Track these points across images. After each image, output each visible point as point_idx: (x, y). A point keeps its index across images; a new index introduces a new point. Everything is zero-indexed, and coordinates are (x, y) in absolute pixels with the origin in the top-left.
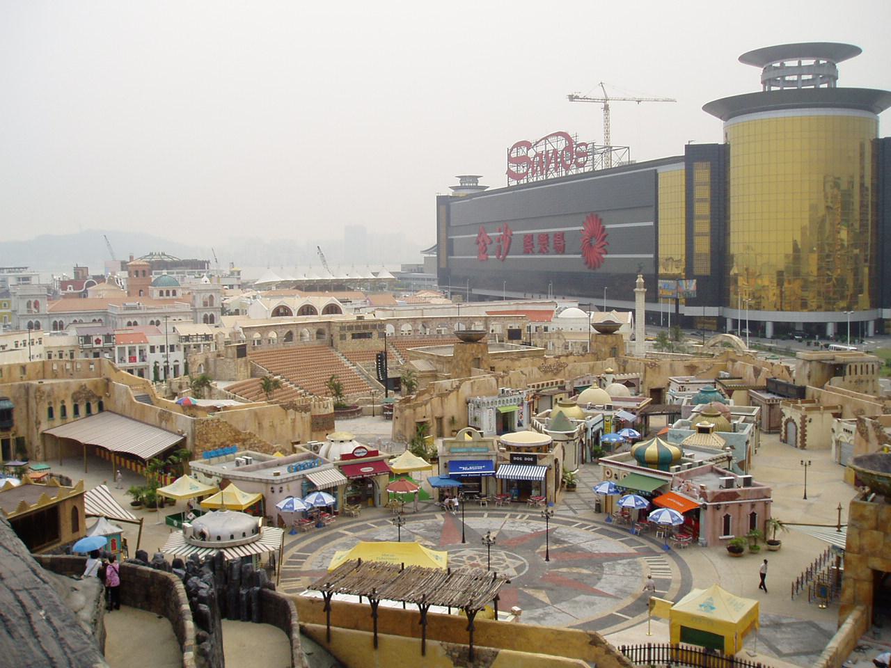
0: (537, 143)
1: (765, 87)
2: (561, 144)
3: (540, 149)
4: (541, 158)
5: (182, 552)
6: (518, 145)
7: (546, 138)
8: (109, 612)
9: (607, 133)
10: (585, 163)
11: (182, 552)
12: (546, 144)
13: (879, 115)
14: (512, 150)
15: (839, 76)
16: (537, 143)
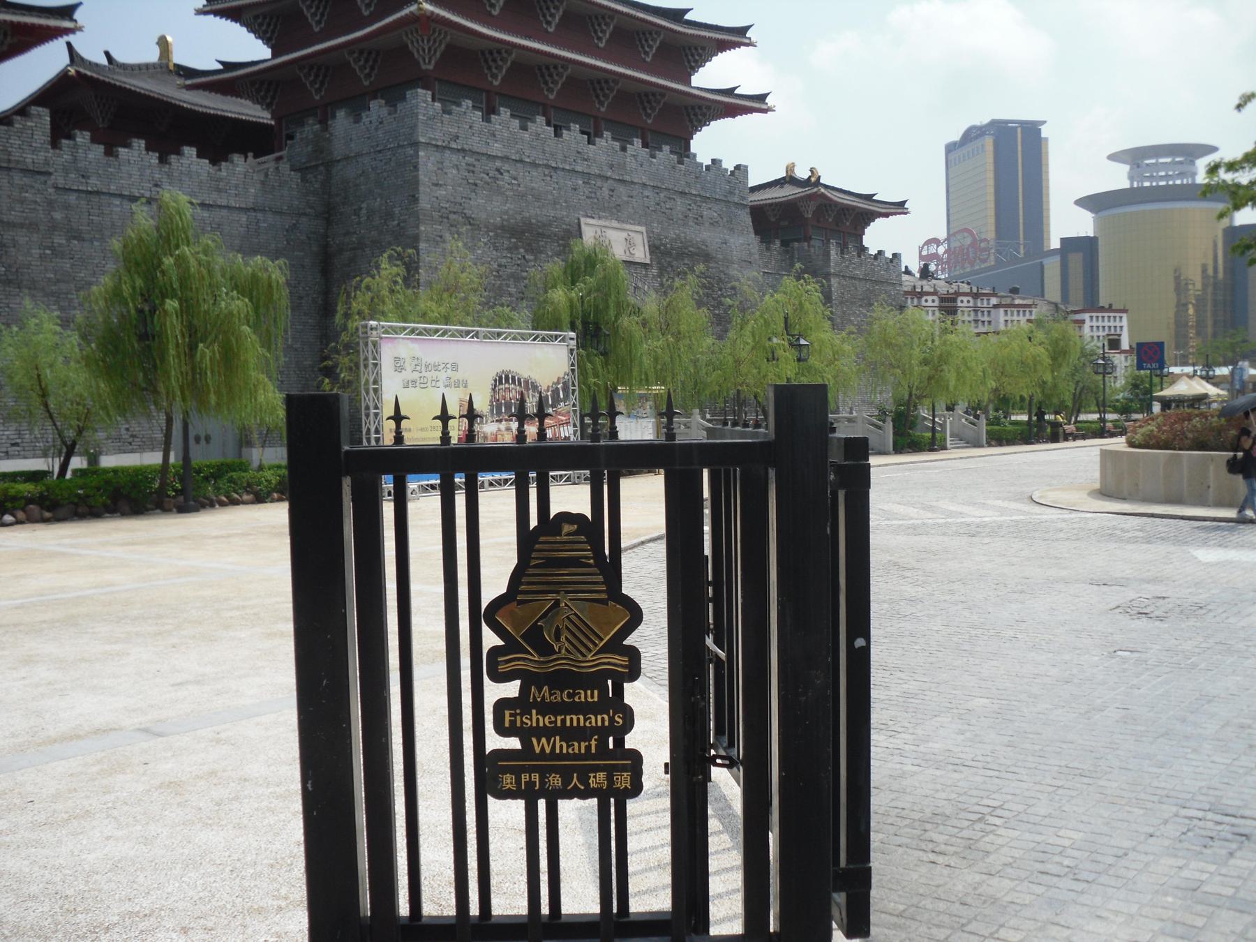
1: (1132, 184)
5: (589, 578)
11: (589, 578)
14: (923, 248)
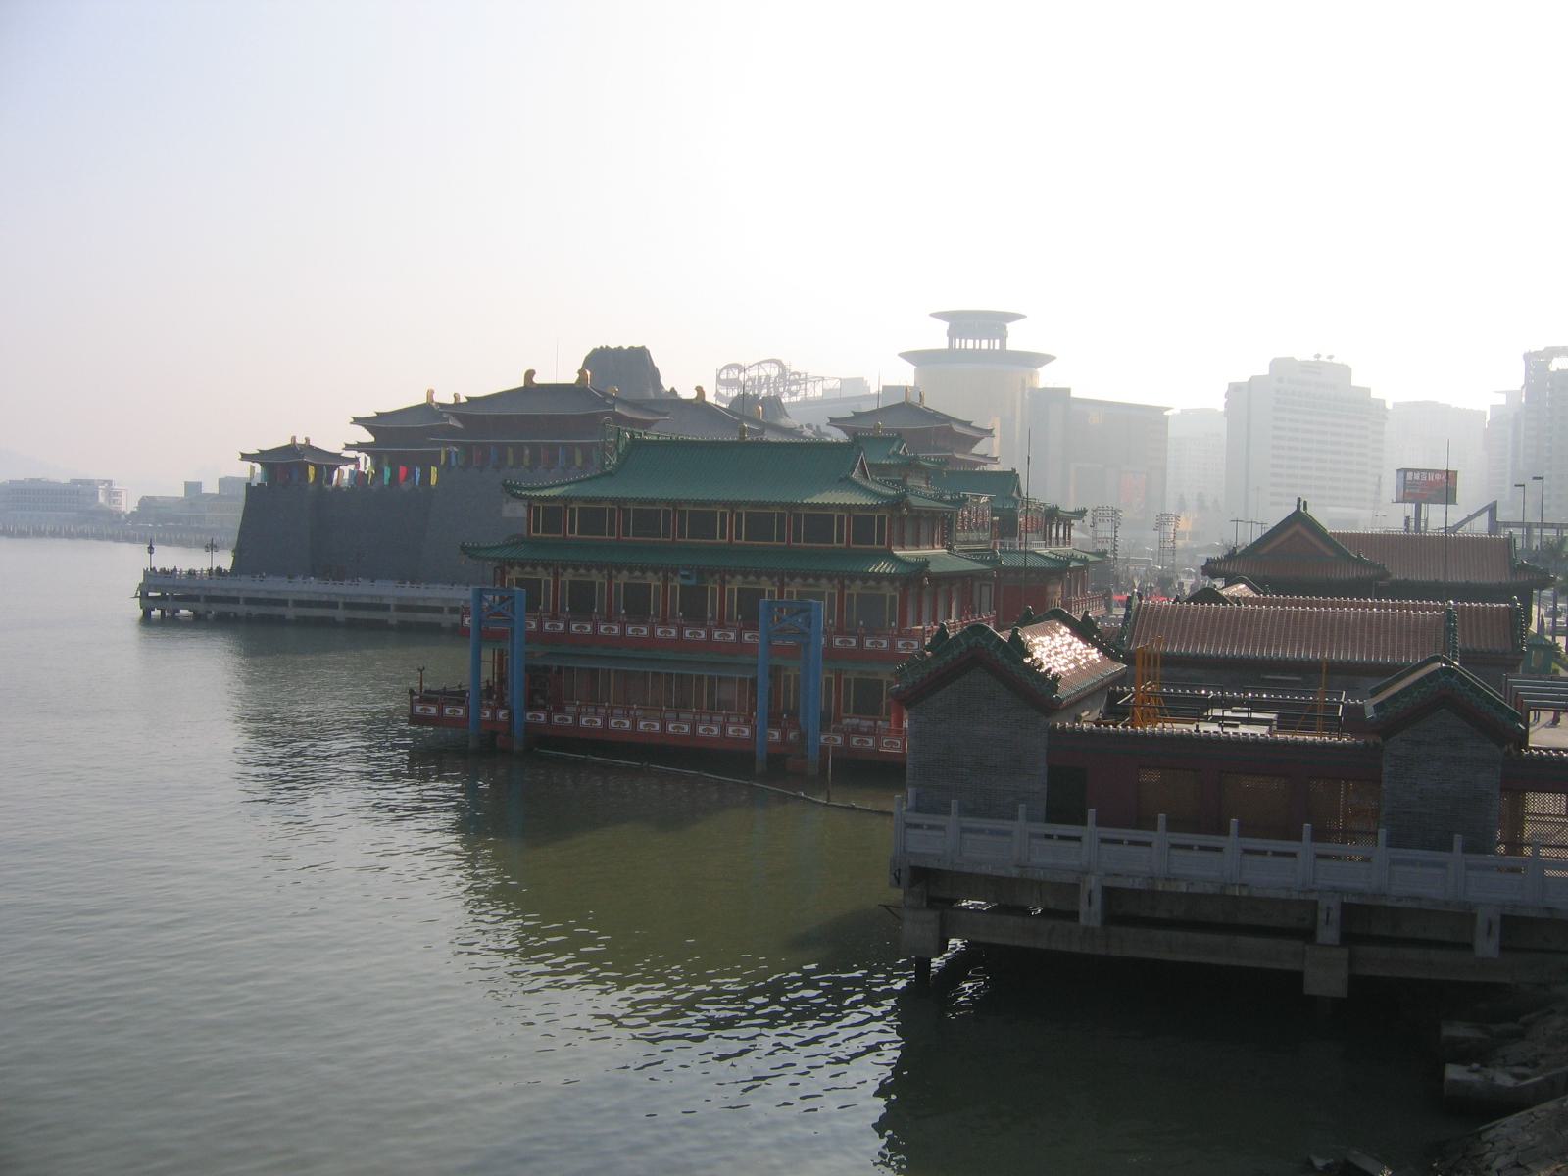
0: (750, 367)
2: (774, 372)
3: (753, 373)
4: (753, 382)
6: (729, 367)
7: (759, 364)
10: (798, 391)
13: (1039, 370)
14: (722, 371)
16: (750, 367)
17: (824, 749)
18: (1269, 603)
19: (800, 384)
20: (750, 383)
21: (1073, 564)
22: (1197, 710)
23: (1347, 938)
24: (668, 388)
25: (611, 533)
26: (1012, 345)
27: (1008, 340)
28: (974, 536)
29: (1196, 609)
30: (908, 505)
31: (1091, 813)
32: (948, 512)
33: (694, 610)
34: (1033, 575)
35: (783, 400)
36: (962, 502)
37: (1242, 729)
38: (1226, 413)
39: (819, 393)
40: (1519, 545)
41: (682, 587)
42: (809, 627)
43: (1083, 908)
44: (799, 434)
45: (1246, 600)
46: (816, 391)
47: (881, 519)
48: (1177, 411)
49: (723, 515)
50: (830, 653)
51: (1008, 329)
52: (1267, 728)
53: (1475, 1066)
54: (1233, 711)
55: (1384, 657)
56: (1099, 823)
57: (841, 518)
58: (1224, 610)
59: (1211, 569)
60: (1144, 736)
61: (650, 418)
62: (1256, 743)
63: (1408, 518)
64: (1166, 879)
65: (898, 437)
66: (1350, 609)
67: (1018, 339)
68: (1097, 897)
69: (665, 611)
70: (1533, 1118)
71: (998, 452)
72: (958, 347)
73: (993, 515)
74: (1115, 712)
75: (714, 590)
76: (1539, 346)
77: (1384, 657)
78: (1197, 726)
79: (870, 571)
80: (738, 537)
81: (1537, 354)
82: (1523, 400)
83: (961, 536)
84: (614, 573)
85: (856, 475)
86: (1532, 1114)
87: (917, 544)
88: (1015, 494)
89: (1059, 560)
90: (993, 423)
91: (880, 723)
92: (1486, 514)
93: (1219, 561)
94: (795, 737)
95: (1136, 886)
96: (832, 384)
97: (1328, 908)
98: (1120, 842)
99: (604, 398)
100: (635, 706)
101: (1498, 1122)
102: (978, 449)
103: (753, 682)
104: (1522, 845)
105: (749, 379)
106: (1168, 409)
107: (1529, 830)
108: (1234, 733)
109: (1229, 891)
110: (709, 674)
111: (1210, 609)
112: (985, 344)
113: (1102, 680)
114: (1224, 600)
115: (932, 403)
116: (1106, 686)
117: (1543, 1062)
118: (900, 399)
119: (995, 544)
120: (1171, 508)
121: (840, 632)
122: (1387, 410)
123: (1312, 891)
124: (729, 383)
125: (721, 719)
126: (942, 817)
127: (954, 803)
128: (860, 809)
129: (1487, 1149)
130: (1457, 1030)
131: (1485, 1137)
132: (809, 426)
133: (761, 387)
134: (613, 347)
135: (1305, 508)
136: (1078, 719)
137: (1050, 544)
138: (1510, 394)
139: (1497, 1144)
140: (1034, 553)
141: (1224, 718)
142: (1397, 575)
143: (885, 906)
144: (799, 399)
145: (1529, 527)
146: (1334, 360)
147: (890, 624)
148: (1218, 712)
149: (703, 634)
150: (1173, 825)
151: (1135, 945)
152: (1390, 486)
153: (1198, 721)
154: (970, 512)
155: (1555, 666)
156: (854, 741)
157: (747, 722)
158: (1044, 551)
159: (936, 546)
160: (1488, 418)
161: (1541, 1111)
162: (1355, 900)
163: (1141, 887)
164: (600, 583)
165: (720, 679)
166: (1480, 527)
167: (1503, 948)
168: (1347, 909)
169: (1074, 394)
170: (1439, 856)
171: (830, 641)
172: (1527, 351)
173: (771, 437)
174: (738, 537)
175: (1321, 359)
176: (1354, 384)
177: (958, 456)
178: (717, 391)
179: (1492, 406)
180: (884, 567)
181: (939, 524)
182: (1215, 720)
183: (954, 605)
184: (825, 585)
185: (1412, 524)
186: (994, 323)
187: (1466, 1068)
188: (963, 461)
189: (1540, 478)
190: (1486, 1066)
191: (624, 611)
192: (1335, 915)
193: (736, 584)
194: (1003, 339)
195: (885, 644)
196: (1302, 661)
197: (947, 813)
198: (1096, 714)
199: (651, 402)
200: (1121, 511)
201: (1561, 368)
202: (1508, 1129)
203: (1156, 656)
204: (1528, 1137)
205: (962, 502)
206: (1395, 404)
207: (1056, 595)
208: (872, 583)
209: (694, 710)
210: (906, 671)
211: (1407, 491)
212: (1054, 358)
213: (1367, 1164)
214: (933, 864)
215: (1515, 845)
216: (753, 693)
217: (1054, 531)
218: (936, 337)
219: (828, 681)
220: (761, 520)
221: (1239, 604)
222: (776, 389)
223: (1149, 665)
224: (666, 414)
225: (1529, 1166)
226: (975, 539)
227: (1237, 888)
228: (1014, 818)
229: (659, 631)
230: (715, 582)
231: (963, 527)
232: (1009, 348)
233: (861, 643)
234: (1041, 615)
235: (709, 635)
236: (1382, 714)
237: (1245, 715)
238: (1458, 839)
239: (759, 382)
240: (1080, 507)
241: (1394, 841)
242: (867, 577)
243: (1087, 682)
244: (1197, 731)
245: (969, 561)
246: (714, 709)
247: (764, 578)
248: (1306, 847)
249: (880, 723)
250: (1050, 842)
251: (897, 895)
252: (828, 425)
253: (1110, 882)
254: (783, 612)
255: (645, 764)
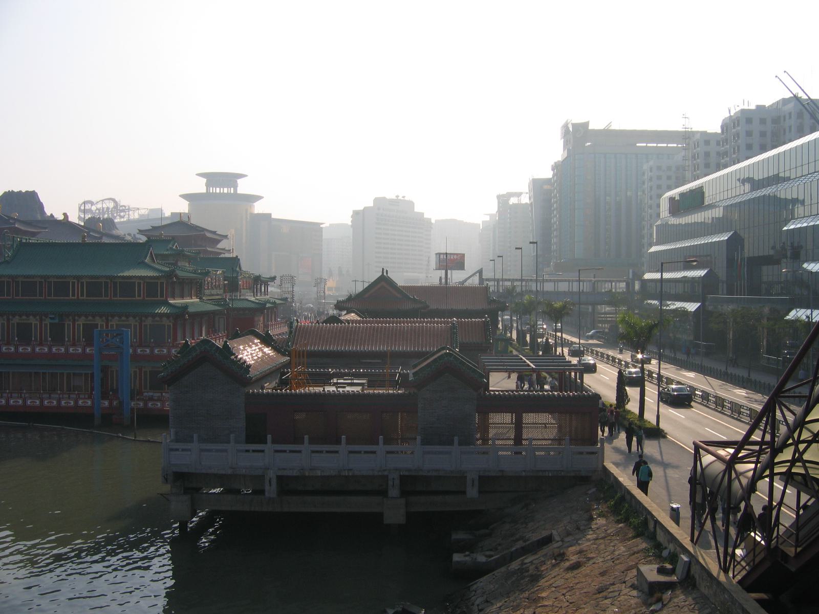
0: (97, 202)
2: (111, 205)
3: (99, 206)
7: (103, 201)
8: (260, 276)
9: (791, 92)
10: (124, 216)
12: (102, 204)
14: (81, 205)
15: (781, 98)
17: (132, 409)
18: (366, 322)
19: (126, 212)
20: (98, 211)
21: (268, 305)
22: (325, 379)
23: (404, 493)
24: (48, 214)
25: (106, 296)
26: (240, 191)
27: (238, 188)
28: (214, 292)
29: (326, 327)
30: (176, 276)
31: (269, 437)
32: (200, 279)
33: (58, 336)
34: (247, 312)
35: (116, 221)
36: (207, 274)
37: (348, 389)
38: (352, 226)
39: (136, 216)
40: (491, 290)
41: (50, 323)
42: (123, 344)
43: (267, 488)
44: (123, 239)
45: (356, 322)
46: (135, 216)
47: (162, 284)
48: (328, 225)
49: (73, 283)
50: (135, 357)
51: (238, 182)
52: (361, 387)
53: (467, 553)
54: (344, 380)
55: (422, 348)
56: (274, 442)
57: (139, 284)
58: (341, 327)
59: (339, 306)
60: (301, 394)
61: (36, 231)
62: (354, 396)
63: (441, 278)
64: (310, 469)
65: (173, 240)
66: (406, 324)
67: (243, 187)
68: (274, 481)
69: (74, 338)
70: (494, 577)
71: (230, 246)
72: (211, 191)
73: (225, 280)
74: (283, 383)
75: (69, 325)
76: (503, 192)
77: (422, 348)
78: (324, 389)
79: (156, 312)
80: (82, 295)
81: (503, 196)
82: (497, 218)
83: (207, 292)
84: (10, 317)
85: (147, 260)
86: (494, 575)
87: (182, 297)
88: (238, 269)
89: (261, 304)
90: (231, 233)
91: (164, 394)
92: (478, 274)
93: (343, 302)
94: (116, 404)
95: (295, 475)
96: (143, 212)
97: (393, 479)
98: (285, 451)
99: (9, 220)
100: (25, 391)
101: (477, 581)
102: (220, 246)
103: (92, 375)
104: (488, 440)
105: (97, 209)
106: (322, 224)
107: (492, 433)
108: (343, 391)
109: (343, 474)
110: (61, 371)
111: (334, 327)
112: (226, 190)
113: (276, 366)
114: (341, 322)
115: (194, 221)
116: (280, 368)
117: (499, 548)
118: (178, 219)
119: (226, 296)
120: (325, 276)
121: (140, 346)
122: (432, 224)
123: (384, 470)
124: (84, 211)
125: (75, 396)
126: (226, 445)
127: (195, 436)
128: (152, 442)
129: (472, 595)
130: (459, 535)
131: (471, 589)
132: (129, 234)
133: (104, 213)
134: (16, 191)
135: (387, 273)
136: (263, 388)
137: (257, 295)
138: (491, 215)
139: (478, 592)
140: (247, 300)
141: (337, 383)
142: (433, 306)
143: (161, 494)
144: (125, 219)
145: (498, 281)
146: (406, 199)
147: (168, 340)
148: (335, 380)
149: (63, 349)
150: (312, 441)
151: (295, 505)
152: (433, 264)
153: (324, 386)
154: (212, 279)
155: (510, 349)
156: (150, 404)
157: (90, 398)
158: (253, 299)
159: (193, 298)
160: (481, 227)
161: (498, 573)
162: (407, 473)
163: (297, 475)
164: (35, 324)
165: (74, 374)
166: (475, 281)
167: (480, 492)
168: (403, 479)
169: (273, 217)
170: (447, 448)
171: (135, 351)
172: (498, 194)
173: (106, 240)
174: (82, 295)
175: (399, 198)
176: (415, 211)
177: (209, 249)
178: (79, 216)
179: (483, 222)
180: (164, 310)
181: (195, 286)
182: (335, 384)
183: (204, 329)
184: (132, 321)
185: (443, 281)
186: (231, 179)
187: (463, 554)
188: (211, 252)
189: (501, 257)
190: (473, 553)
191: (16, 339)
192: (397, 482)
193: (81, 321)
194: (235, 187)
195: (165, 351)
196: (381, 352)
197: (192, 441)
198: (274, 384)
199: (39, 221)
200: (295, 277)
201: (514, 203)
202: (483, 583)
203: (299, 352)
204: (492, 586)
205: (207, 274)
206: (436, 221)
207: (260, 321)
208: (157, 319)
209: (59, 392)
210: (167, 366)
211: (441, 264)
212: (181, 196)
213: (413, 609)
214: (185, 470)
215: (485, 440)
216: (92, 380)
217: (263, 288)
218: (200, 186)
219: (135, 372)
220: (95, 286)
221: (349, 323)
222: (112, 214)
223: (299, 357)
224: (45, 228)
225: (492, 601)
226: (216, 293)
227: (346, 471)
228: (228, 442)
229: (71, 349)
230: (70, 320)
231: (208, 287)
232: (238, 192)
233: (152, 351)
234: (244, 333)
235: (67, 350)
236: (416, 378)
237: (350, 381)
238: (456, 439)
239: (102, 211)
240: (273, 275)
241: (426, 442)
242: (154, 316)
243: (267, 368)
244: (324, 390)
245: (212, 305)
246: (70, 391)
247: (31, 317)
248: (381, 448)
249: (164, 394)
250: (247, 454)
251: (166, 488)
252: (138, 233)
253: (280, 473)
254: (108, 336)
255: (31, 424)
